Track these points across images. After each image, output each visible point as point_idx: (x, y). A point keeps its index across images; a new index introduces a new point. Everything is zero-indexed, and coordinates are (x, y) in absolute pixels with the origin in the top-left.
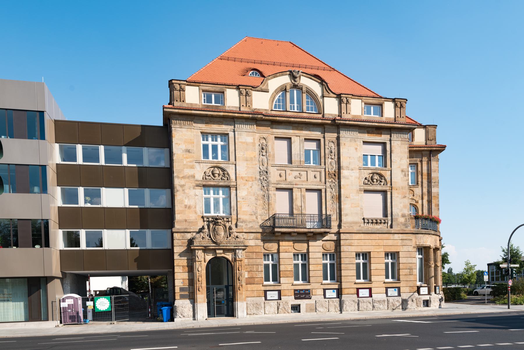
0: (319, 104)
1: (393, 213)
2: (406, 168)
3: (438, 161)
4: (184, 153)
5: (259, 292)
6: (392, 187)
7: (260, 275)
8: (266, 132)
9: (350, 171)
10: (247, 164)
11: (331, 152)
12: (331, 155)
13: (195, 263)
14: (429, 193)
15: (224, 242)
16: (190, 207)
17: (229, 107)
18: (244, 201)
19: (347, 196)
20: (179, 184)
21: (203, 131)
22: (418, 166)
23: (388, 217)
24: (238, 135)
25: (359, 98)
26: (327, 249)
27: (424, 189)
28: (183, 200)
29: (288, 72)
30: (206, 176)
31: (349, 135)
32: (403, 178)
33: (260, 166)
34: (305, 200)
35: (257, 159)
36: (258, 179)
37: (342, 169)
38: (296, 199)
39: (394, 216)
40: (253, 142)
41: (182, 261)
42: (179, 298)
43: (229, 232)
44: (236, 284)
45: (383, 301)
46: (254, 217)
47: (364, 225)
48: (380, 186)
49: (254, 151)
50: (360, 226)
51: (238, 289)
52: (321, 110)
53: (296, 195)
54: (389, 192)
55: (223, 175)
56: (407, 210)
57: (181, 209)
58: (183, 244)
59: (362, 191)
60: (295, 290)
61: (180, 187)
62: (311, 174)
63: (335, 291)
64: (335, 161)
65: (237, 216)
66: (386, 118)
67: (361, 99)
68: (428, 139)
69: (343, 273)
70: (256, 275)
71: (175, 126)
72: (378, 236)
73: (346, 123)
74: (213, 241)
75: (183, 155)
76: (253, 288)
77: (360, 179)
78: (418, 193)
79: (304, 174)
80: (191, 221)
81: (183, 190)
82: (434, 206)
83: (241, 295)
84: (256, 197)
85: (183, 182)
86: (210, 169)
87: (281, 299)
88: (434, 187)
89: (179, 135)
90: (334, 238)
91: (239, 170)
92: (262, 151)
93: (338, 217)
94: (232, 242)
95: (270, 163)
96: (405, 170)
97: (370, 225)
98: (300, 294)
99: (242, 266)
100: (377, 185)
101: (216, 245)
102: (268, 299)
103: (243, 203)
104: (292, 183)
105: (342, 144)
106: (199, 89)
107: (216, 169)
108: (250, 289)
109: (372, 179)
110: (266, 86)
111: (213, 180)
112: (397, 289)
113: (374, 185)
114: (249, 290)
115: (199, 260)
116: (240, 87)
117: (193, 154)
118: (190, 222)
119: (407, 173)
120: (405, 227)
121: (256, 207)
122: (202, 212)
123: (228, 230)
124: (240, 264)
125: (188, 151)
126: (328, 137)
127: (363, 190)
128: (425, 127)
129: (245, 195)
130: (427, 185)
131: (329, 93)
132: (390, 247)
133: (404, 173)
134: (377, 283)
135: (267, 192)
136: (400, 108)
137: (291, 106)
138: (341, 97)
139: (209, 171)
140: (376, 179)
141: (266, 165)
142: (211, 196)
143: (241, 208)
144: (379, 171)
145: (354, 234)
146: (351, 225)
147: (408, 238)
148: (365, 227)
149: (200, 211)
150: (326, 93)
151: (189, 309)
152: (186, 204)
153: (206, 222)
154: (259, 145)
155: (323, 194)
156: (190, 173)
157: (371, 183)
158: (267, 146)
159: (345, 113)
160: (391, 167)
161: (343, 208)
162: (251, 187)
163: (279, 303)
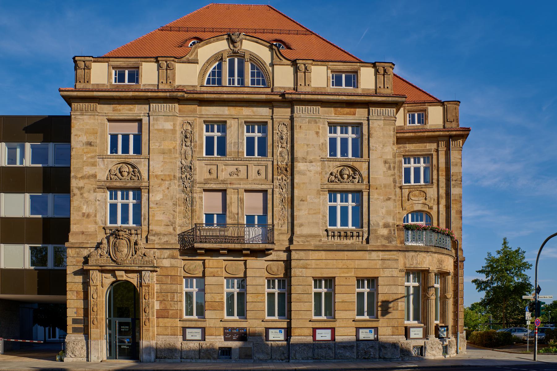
0: (268, 75)
1: (370, 222)
2: (391, 157)
3: (461, 150)
4: (84, 147)
5: (174, 329)
6: (369, 185)
7: (176, 306)
8: (192, 115)
9: (308, 164)
10: (164, 158)
11: (282, 139)
12: (281, 143)
13: (89, 287)
14: (448, 194)
15: (128, 262)
16: (88, 216)
17: (144, 85)
18: (158, 207)
19: (303, 199)
20: (76, 185)
21: (110, 117)
22: (432, 158)
23: (364, 229)
24: (154, 121)
25: (324, 63)
26: (273, 272)
27: (440, 189)
28: (80, 206)
29: (225, 36)
30: (111, 175)
31: (307, 114)
32: (386, 173)
33: (183, 160)
34: (243, 206)
35: (178, 151)
36: (179, 178)
37: (296, 161)
38: (231, 203)
39: (372, 226)
40: (172, 128)
41: (76, 285)
42: (71, 332)
43: (135, 248)
44: (141, 317)
45: (350, 346)
46: (171, 229)
47: (328, 239)
48: (352, 184)
49: (174, 140)
50: (320, 241)
51: (143, 324)
52: (270, 82)
53: (231, 198)
54: (365, 191)
55: (133, 173)
56: (392, 218)
57: (78, 218)
58: (78, 263)
59: (326, 191)
60: (225, 329)
61: (77, 190)
62: (253, 170)
63: (283, 330)
64: (288, 150)
65: (149, 227)
66: (363, 89)
67: (326, 65)
68: (447, 120)
69: (294, 306)
70: (171, 306)
71: (75, 113)
72: (347, 255)
73: (300, 99)
74: (112, 259)
75: (83, 150)
76: (166, 323)
77: (323, 174)
78: (432, 195)
79: (243, 169)
80: (90, 233)
81: (81, 194)
82: (455, 214)
83: (147, 331)
84: (174, 201)
85: (81, 183)
86: (117, 166)
87: (205, 340)
88: (454, 187)
89: (80, 124)
90: (284, 256)
91: (153, 167)
92: (186, 139)
93: (290, 228)
94: (138, 261)
95: (196, 155)
96: (389, 161)
97: (337, 240)
98: (232, 334)
99: (150, 294)
100: (348, 182)
101: (117, 265)
102: (187, 339)
103: (156, 209)
104: (225, 182)
105: (296, 127)
106: (108, 65)
107: (124, 165)
108: (163, 325)
109: (341, 175)
110: (195, 56)
111: (120, 180)
112: (373, 330)
113: (344, 182)
114: (161, 325)
115: (94, 284)
116: (159, 59)
117: (95, 148)
118: (87, 235)
119: (392, 165)
120: (387, 242)
121: (173, 215)
122: (103, 223)
123: (133, 246)
124: (147, 291)
125: (90, 144)
126: (277, 118)
127: (327, 190)
128: (442, 104)
129: (159, 199)
130: (446, 184)
131: (280, 59)
132: (365, 270)
133: (387, 165)
134: (343, 321)
135: (190, 194)
136: (384, 75)
137: (230, 80)
138: (297, 64)
139: (116, 169)
140: (348, 175)
141: (190, 159)
142: (119, 201)
143: (153, 216)
144: (352, 162)
145: (311, 252)
146: (307, 239)
147: (391, 258)
148: (329, 242)
149: (102, 220)
150: (276, 60)
151: (82, 347)
153: (134, 235)
154: (182, 132)
155: (269, 197)
156: (90, 172)
157: (338, 181)
158: (192, 134)
159: (303, 84)
160: (369, 157)
161: (296, 215)
162: (168, 188)
163: (201, 344)
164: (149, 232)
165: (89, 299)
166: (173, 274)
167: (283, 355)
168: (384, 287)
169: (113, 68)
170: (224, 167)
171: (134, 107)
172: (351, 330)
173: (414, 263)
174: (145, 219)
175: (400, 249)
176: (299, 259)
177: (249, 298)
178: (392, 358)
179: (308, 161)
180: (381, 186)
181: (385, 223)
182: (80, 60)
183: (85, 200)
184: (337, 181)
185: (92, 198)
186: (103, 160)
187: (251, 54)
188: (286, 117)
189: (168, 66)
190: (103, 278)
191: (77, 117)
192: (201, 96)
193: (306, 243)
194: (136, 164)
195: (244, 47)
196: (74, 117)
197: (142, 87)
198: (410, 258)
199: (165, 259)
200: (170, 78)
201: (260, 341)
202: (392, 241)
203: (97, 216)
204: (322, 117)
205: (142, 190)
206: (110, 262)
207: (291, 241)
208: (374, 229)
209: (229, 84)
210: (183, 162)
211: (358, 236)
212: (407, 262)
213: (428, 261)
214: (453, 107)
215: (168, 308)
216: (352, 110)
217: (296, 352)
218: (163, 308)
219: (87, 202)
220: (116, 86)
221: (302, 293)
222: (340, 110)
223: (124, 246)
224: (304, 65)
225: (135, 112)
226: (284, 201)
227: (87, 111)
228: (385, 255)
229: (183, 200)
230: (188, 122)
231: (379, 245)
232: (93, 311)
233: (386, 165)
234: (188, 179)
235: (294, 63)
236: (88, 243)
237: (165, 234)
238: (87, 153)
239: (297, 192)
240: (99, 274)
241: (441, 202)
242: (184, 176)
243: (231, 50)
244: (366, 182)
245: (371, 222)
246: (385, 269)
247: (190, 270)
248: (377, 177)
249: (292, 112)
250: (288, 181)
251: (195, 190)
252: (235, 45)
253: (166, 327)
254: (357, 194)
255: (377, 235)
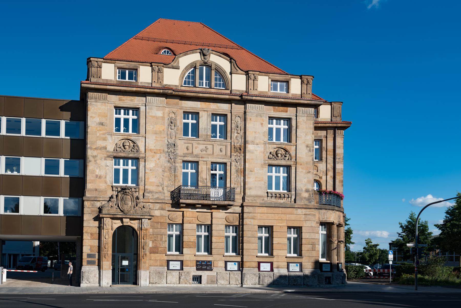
4: (97, 126)
5: (162, 262)
7: (164, 245)
8: (176, 107)
9: (255, 145)
16: (100, 177)
17: (141, 83)
18: (151, 173)
19: (252, 170)
24: (149, 110)
25: (266, 74)
26: (230, 221)
29: (198, 50)
30: (117, 148)
31: (256, 110)
32: (307, 154)
33: (169, 139)
35: (166, 132)
37: (248, 144)
38: (202, 171)
41: (91, 229)
42: (86, 264)
47: (268, 199)
48: (284, 161)
49: (163, 125)
50: (263, 200)
51: (142, 258)
53: (202, 168)
55: (133, 147)
56: (311, 185)
60: (197, 261)
61: (92, 158)
62: (217, 149)
66: (293, 94)
70: (160, 245)
71: (90, 100)
72: (281, 211)
75: (97, 128)
76: (156, 257)
77: (265, 153)
78: (322, 168)
79: (210, 147)
81: (95, 161)
83: (145, 263)
84: (163, 168)
85: (95, 153)
87: (183, 270)
88: (338, 163)
89: (94, 109)
90: (239, 210)
91: (149, 143)
92: (171, 124)
94: (138, 212)
96: (309, 145)
97: (274, 200)
98: (202, 265)
99: (147, 235)
100: (282, 160)
101: (124, 214)
104: (198, 156)
105: (248, 119)
108: (154, 259)
110: (177, 63)
111: (124, 151)
114: (152, 259)
115: (106, 228)
116: (153, 64)
118: (99, 191)
119: (311, 149)
121: (163, 179)
125: (102, 124)
127: (268, 164)
129: (152, 167)
133: (308, 148)
135: (174, 164)
137: (200, 82)
143: (148, 179)
144: (284, 146)
145: (257, 208)
146: (254, 198)
147: (311, 213)
148: (268, 201)
149: (110, 181)
152: (97, 174)
154: (168, 119)
155: (228, 168)
156: (102, 145)
159: (252, 89)
160: (296, 142)
161: (247, 181)
162: (159, 159)
164: (145, 190)
165: (102, 239)
166: (162, 221)
167: (237, 281)
168: (306, 234)
169: (118, 68)
170: (197, 145)
171: (134, 98)
172: (284, 264)
173: (325, 217)
174: (141, 181)
175: (317, 208)
176: (249, 212)
177: (214, 239)
178: (312, 285)
179: (255, 143)
180: (304, 163)
181: (306, 189)
182: (94, 61)
183: (98, 166)
184: (274, 158)
185: (104, 164)
186: (111, 136)
187: (216, 65)
188: (240, 112)
189: (159, 69)
190: (113, 224)
191: (92, 103)
192: (184, 94)
193: (254, 201)
194: (136, 140)
195: (211, 59)
196: (90, 103)
197: (140, 84)
198: (322, 214)
199: (156, 210)
200: (160, 79)
201: (222, 271)
202: (311, 202)
203: (107, 177)
204: (265, 113)
205: (140, 160)
206: (119, 211)
207: (243, 199)
208: (299, 193)
209: (200, 85)
210: (169, 141)
211: (288, 197)
212: (321, 217)
213: (333, 216)
214: (338, 106)
215: (158, 246)
216: (285, 108)
217: (247, 279)
218: (154, 246)
219: (100, 167)
220: (120, 82)
221: (251, 236)
222: (277, 108)
223: (129, 200)
224: (253, 75)
225: (135, 102)
226: (238, 171)
227: (100, 99)
228: (307, 211)
229: (168, 167)
230: (173, 112)
231: (303, 204)
232: (105, 248)
233: (308, 148)
234: (172, 153)
235: (247, 73)
236: (100, 197)
237: (156, 192)
238: (100, 130)
239: (248, 165)
240: (110, 220)
241: (329, 174)
242: (169, 151)
243: (203, 61)
244: (294, 160)
245: (297, 188)
246: (307, 222)
247: (173, 219)
248: (301, 156)
249: (245, 108)
250: (241, 157)
251: (177, 161)
252: (205, 58)
253: (156, 260)
254: (288, 168)
255: (301, 197)
